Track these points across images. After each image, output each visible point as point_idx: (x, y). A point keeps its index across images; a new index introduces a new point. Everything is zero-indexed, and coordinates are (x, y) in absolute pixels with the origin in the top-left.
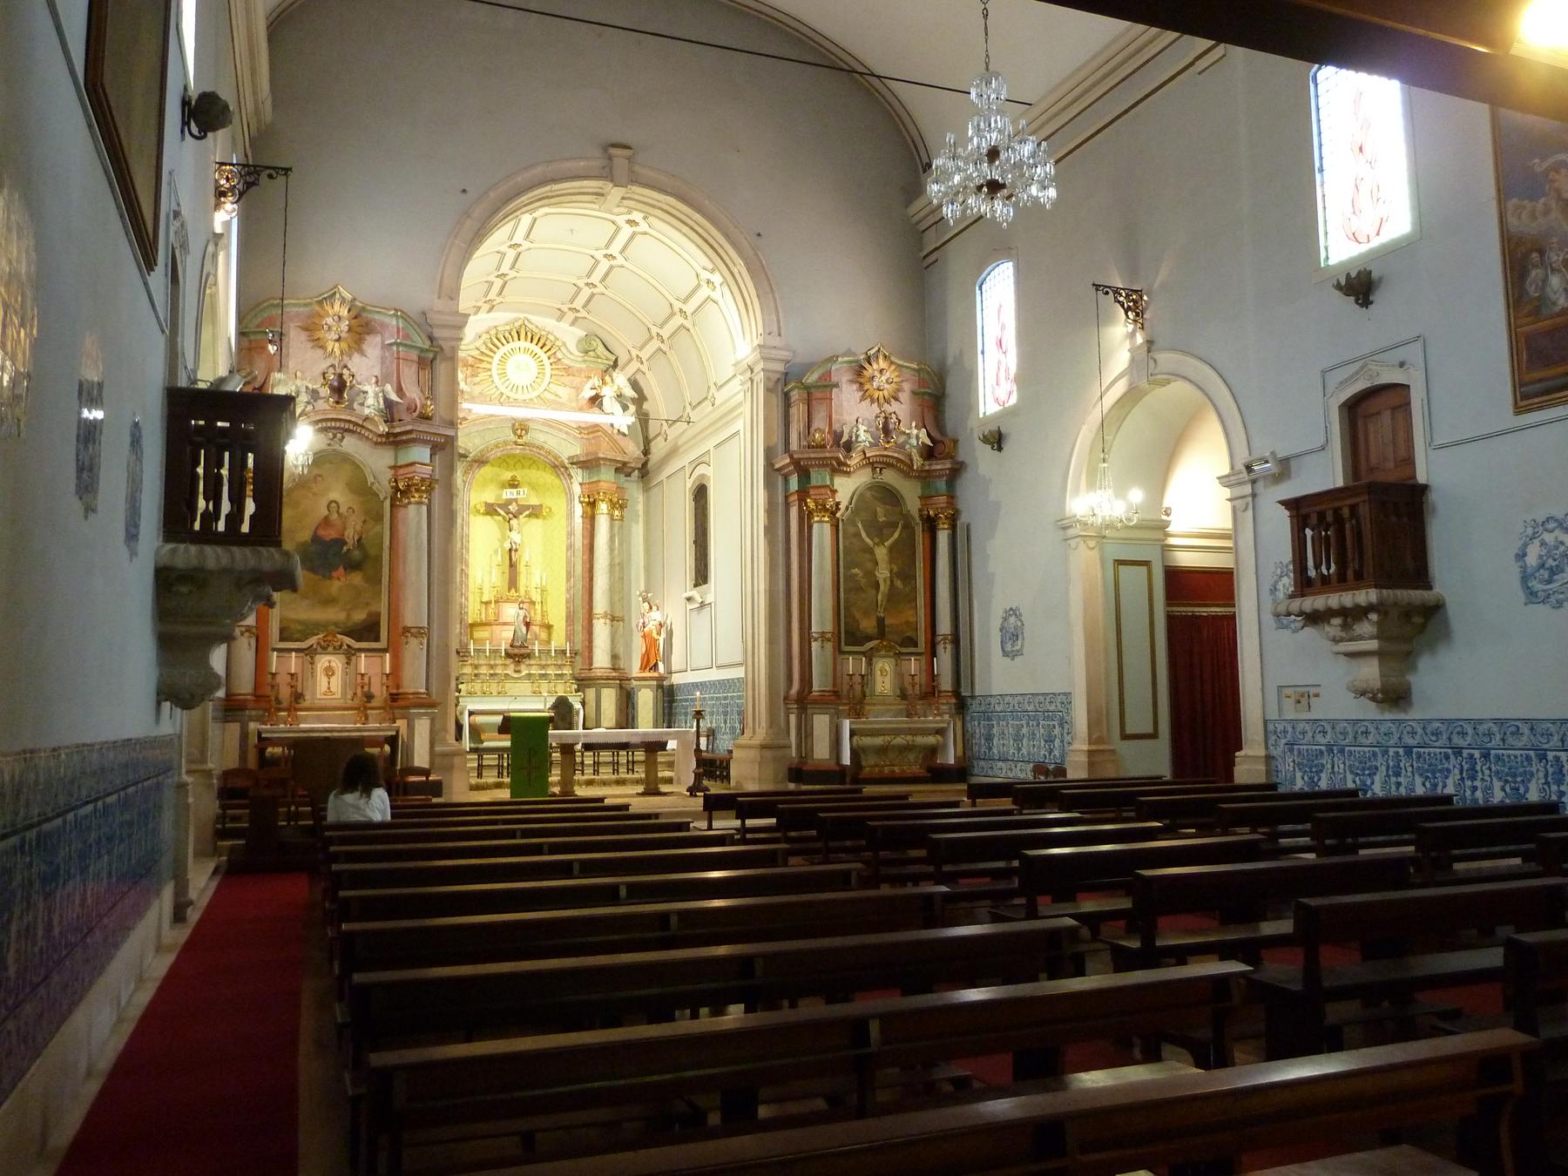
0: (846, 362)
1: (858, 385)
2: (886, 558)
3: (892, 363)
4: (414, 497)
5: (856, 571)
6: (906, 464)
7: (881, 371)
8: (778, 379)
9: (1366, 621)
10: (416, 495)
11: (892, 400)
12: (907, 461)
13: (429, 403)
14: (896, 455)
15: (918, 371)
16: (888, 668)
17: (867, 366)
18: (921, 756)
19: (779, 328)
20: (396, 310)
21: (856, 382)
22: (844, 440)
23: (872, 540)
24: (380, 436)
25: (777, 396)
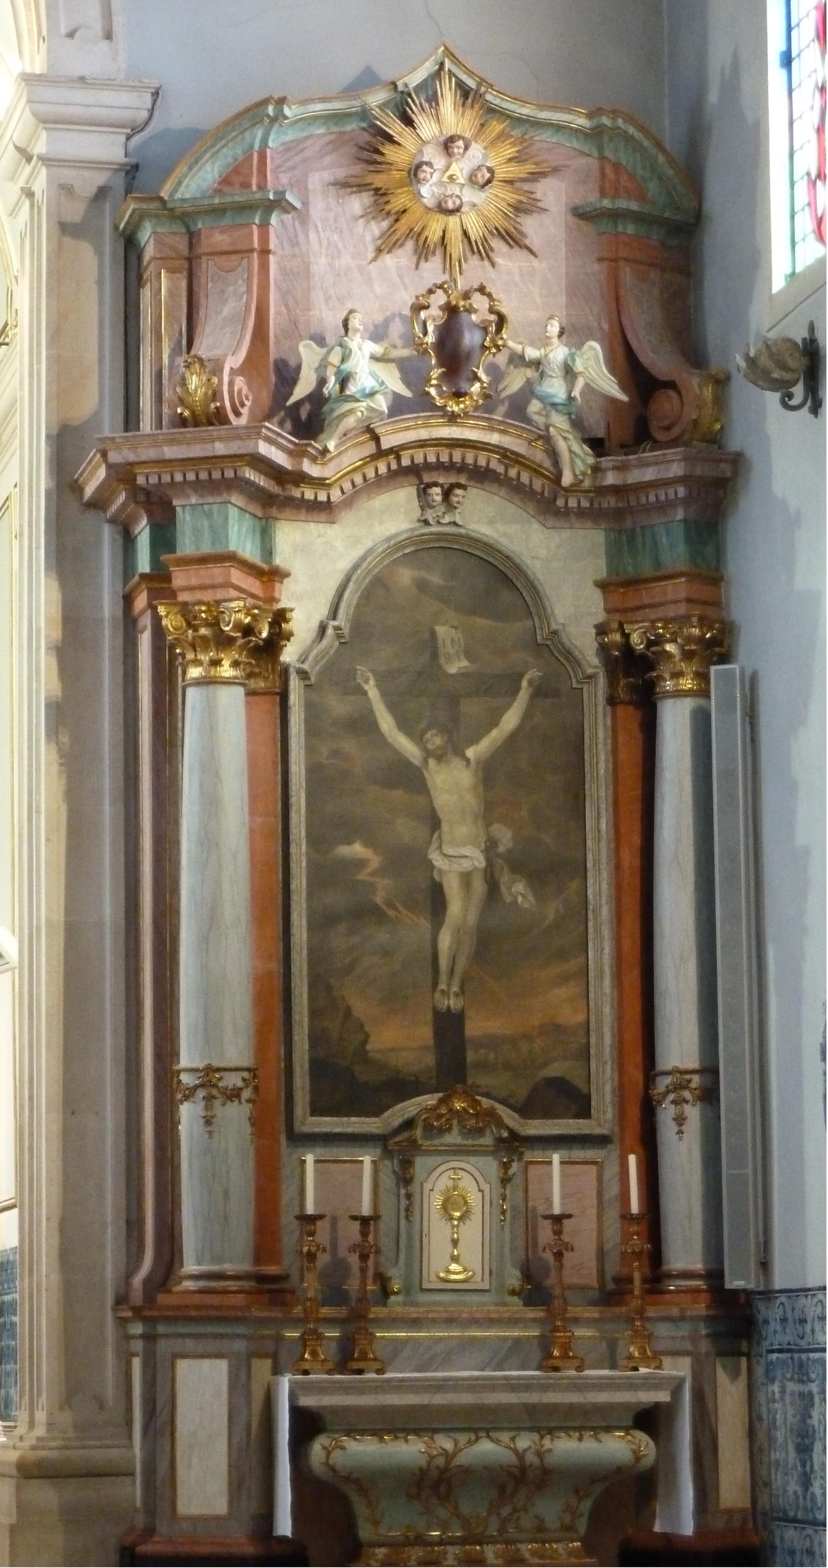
0: (314, 119)
2: (471, 801)
3: (492, 111)
5: (357, 849)
6: (536, 470)
7: (447, 145)
11: (497, 244)
12: (547, 463)
14: (494, 438)
15: (595, 135)
16: (474, 1199)
17: (395, 128)
18: (586, 1506)
21: (362, 187)
22: (301, 391)
23: (418, 738)
25: (99, 253)
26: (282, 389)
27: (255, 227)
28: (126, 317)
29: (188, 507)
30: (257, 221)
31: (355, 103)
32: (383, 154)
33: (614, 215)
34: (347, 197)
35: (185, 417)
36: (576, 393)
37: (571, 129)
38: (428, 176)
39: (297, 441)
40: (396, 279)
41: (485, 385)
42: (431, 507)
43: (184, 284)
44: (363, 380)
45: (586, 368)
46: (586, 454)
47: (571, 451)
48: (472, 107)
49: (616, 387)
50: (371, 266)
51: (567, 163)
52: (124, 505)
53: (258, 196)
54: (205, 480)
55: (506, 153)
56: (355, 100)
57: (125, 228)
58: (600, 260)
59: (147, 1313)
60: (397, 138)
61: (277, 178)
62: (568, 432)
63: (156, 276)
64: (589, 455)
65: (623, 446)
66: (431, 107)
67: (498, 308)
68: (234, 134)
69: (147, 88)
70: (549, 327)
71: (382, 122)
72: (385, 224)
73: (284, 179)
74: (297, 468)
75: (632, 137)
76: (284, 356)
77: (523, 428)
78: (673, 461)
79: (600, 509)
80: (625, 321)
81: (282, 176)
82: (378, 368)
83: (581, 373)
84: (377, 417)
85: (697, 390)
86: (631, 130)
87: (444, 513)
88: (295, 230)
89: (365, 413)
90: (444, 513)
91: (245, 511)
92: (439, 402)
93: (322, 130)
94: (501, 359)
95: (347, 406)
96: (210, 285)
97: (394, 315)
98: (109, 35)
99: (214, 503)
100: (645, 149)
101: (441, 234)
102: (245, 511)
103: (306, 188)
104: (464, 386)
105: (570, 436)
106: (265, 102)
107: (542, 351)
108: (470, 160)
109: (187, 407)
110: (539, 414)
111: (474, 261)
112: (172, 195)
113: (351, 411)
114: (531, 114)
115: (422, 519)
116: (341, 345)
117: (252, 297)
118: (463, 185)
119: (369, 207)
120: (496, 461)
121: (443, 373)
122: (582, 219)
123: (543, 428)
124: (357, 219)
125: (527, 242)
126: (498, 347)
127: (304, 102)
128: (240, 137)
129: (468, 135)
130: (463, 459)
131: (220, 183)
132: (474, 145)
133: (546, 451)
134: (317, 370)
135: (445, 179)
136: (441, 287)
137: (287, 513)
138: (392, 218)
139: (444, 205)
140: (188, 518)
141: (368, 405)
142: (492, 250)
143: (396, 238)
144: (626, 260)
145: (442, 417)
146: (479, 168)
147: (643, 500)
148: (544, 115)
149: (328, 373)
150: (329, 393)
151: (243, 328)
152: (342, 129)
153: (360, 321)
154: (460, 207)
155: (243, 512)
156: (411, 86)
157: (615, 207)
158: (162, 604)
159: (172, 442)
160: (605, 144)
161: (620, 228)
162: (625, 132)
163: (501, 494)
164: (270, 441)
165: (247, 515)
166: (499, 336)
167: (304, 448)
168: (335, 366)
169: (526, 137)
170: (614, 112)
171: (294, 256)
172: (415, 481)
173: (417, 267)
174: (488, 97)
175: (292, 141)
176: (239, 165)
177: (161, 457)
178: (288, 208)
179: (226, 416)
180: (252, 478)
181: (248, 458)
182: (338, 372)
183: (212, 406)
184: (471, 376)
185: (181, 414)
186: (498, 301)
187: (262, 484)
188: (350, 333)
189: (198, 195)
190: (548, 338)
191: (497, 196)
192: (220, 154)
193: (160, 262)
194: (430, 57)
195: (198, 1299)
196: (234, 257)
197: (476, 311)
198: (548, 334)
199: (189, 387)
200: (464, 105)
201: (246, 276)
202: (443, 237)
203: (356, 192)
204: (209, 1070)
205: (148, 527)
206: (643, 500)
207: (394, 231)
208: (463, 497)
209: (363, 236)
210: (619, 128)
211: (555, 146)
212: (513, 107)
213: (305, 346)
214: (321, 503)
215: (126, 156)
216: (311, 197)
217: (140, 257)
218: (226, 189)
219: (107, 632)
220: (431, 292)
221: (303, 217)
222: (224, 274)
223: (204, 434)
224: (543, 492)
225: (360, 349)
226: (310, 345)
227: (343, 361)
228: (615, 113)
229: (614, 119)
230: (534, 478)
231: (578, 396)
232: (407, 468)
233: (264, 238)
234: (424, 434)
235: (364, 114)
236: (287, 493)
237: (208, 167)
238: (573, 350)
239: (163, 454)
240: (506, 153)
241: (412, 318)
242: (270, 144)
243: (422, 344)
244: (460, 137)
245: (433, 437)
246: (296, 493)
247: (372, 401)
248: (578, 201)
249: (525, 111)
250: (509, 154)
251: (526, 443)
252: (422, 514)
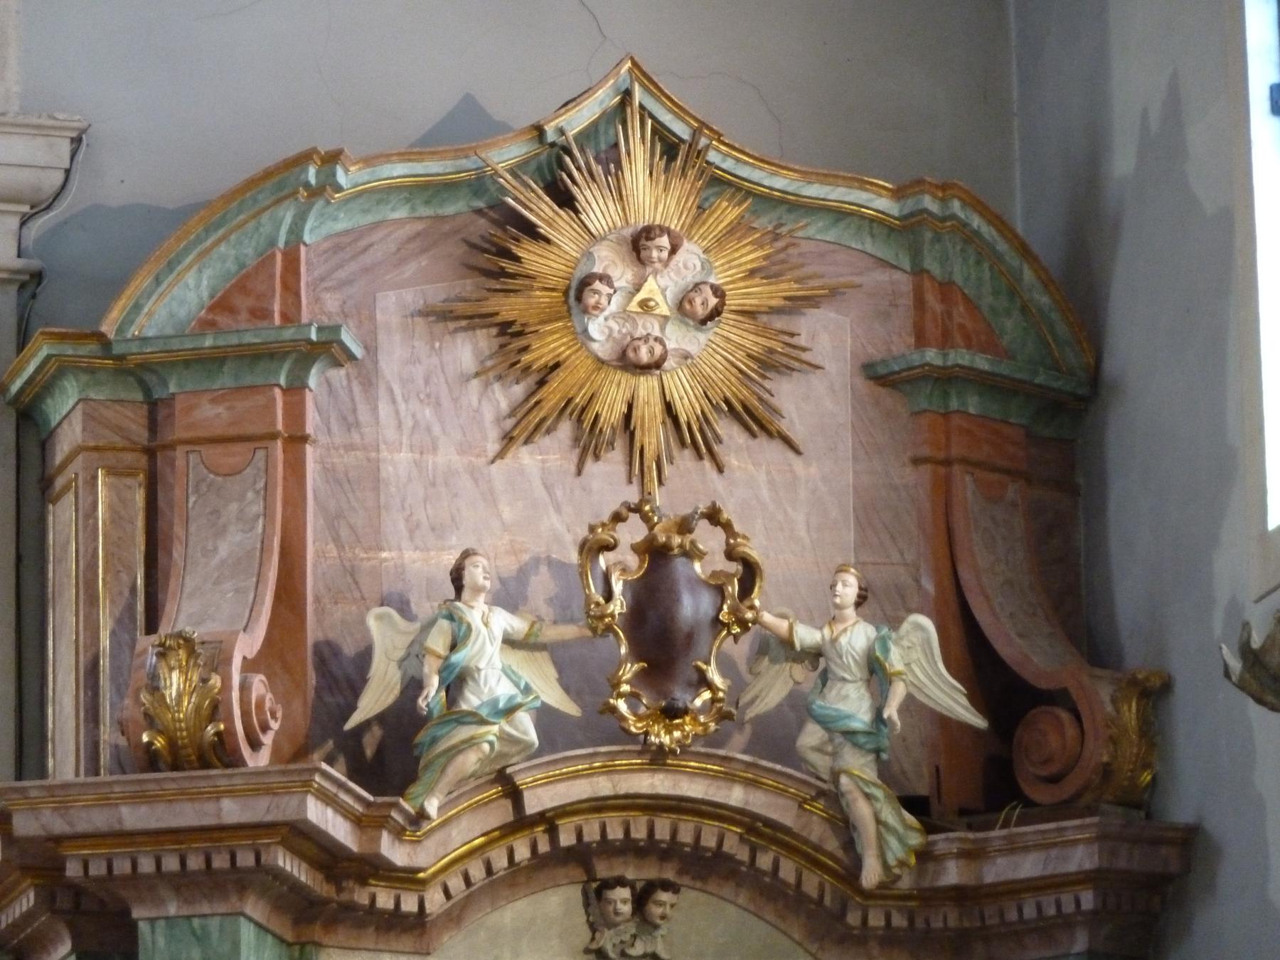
0: (386, 193)
1: (485, 340)
3: (718, 183)
6: (809, 856)
9: (516, 629)
11: (727, 429)
12: (832, 845)
14: (736, 796)
17: (541, 210)
21: (476, 320)
26: (329, 699)
27: (277, 391)
28: (19, 559)
29: (162, 923)
30: (282, 381)
31: (464, 163)
32: (517, 259)
33: (946, 379)
34: (447, 337)
35: (156, 752)
36: (891, 711)
37: (863, 217)
38: (604, 301)
39: (371, 798)
40: (540, 492)
41: (721, 694)
42: (611, 925)
43: (140, 497)
44: (492, 681)
45: (908, 665)
46: (908, 827)
47: (878, 821)
48: (684, 174)
49: (964, 701)
50: (494, 467)
51: (857, 280)
52: (28, 917)
53: (288, 334)
54: (199, 871)
55: (744, 260)
56: (466, 157)
57: (22, 391)
58: (916, 461)
60: (544, 229)
61: (317, 300)
62: (875, 785)
63: (86, 482)
64: (910, 828)
65: (963, 812)
66: (607, 172)
67: (747, 550)
68: (242, 217)
69: (61, 128)
70: (839, 587)
71: (515, 199)
72: (519, 390)
73: (332, 302)
74: (368, 849)
75: (977, 233)
76: (331, 636)
77: (790, 777)
78: (1075, 843)
79: (928, 930)
80: (966, 575)
81: (327, 296)
82: (517, 659)
83: (899, 674)
84: (519, 753)
85: (1109, 708)
86: (976, 222)
87: (634, 937)
88: (353, 400)
89: (497, 746)
90: (634, 937)
91: (267, 930)
92: (635, 727)
93: (402, 213)
94: (740, 650)
95: (464, 733)
96: (192, 499)
97: (537, 561)
99: (213, 915)
100: (999, 257)
101: (625, 409)
102: (267, 930)
103: (372, 318)
104: (681, 696)
105: (879, 793)
106: (302, 159)
107: (826, 631)
108: (678, 272)
109: (160, 732)
110: (819, 749)
111: (685, 459)
112: (120, 330)
113: (471, 743)
114: (790, 189)
115: (594, 946)
116: (451, 617)
117: (273, 523)
118: (666, 318)
119: (491, 357)
120: (737, 838)
121: (643, 670)
122: (883, 385)
123: (826, 777)
124: (468, 380)
125: (784, 426)
126: (744, 624)
127: (369, 161)
128: (252, 224)
129: (674, 225)
130: (674, 833)
131: (211, 309)
132: (686, 245)
133: (830, 821)
134: (401, 662)
135: (634, 307)
136: (637, 509)
137: (341, 935)
138: (532, 380)
139: (631, 354)
140: (161, 942)
141: (501, 730)
142: (719, 440)
143: (542, 414)
144: (964, 461)
145: (640, 754)
146: (696, 287)
147: (1012, 916)
148: (814, 191)
149: (426, 669)
150: (428, 706)
152: (440, 212)
153: (485, 570)
154: (663, 358)
155: (262, 933)
156: (571, 133)
157: (949, 363)
159: (139, 798)
160: (926, 247)
161: (954, 404)
162: (965, 225)
163: (741, 901)
164: (328, 799)
165: (270, 938)
166: (747, 603)
167: (384, 812)
168: (439, 657)
169: (784, 230)
170: (944, 187)
171: (350, 447)
172: (579, 874)
173: (579, 472)
174: (712, 156)
175: (347, 232)
176: (247, 276)
177: (117, 827)
178: (341, 357)
179: (236, 751)
180: (288, 868)
181: (284, 830)
182: (445, 670)
183: (210, 730)
184: (695, 677)
185: (150, 744)
186: (745, 537)
187: (303, 879)
188: (466, 594)
189: (169, 331)
190: (839, 607)
191: (728, 340)
192: (214, 255)
193: (95, 455)
194: (605, 78)
196: (238, 448)
197: (701, 555)
198: (838, 600)
199: (167, 693)
200: (667, 169)
201: (261, 484)
202: (628, 417)
203: (465, 329)
206: (1012, 916)
207: (537, 403)
208: (672, 906)
209: (477, 411)
210: (953, 217)
211: (832, 247)
212: (756, 175)
213: (380, 618)
214: (407, 915)
215: (19, 256)
216: (382, 337)
217: (45, 444)
218: (223, 320)
220: (617, 518)
221: (368, 378)
222: (220, 479)
223: (203, 783)
224: (822, 896)
225: (486, 624)
226: (390, 616)
227: (453, 647)
228: (945, 190)
229: (944, 201)
230: (805, 873)
231: (895, 717)
232: (569, 849)
233: (296, 414)
234: (603, 786)
235: (480, 183)
236: (344, 897)
237: (190, 278)
238: (885, 631)
239: (120, 821)
240: (744, 260)
241: (582, 566)
242: (307, 238)
243: (602, 617)
244: (664, 230)
245: (622, 792)
246: (361, 897)
247: (510, 723)
248: (875, 353)
249: (780, 182)
250: (752, 261)
251: (793, 806)
252: (593, 939)
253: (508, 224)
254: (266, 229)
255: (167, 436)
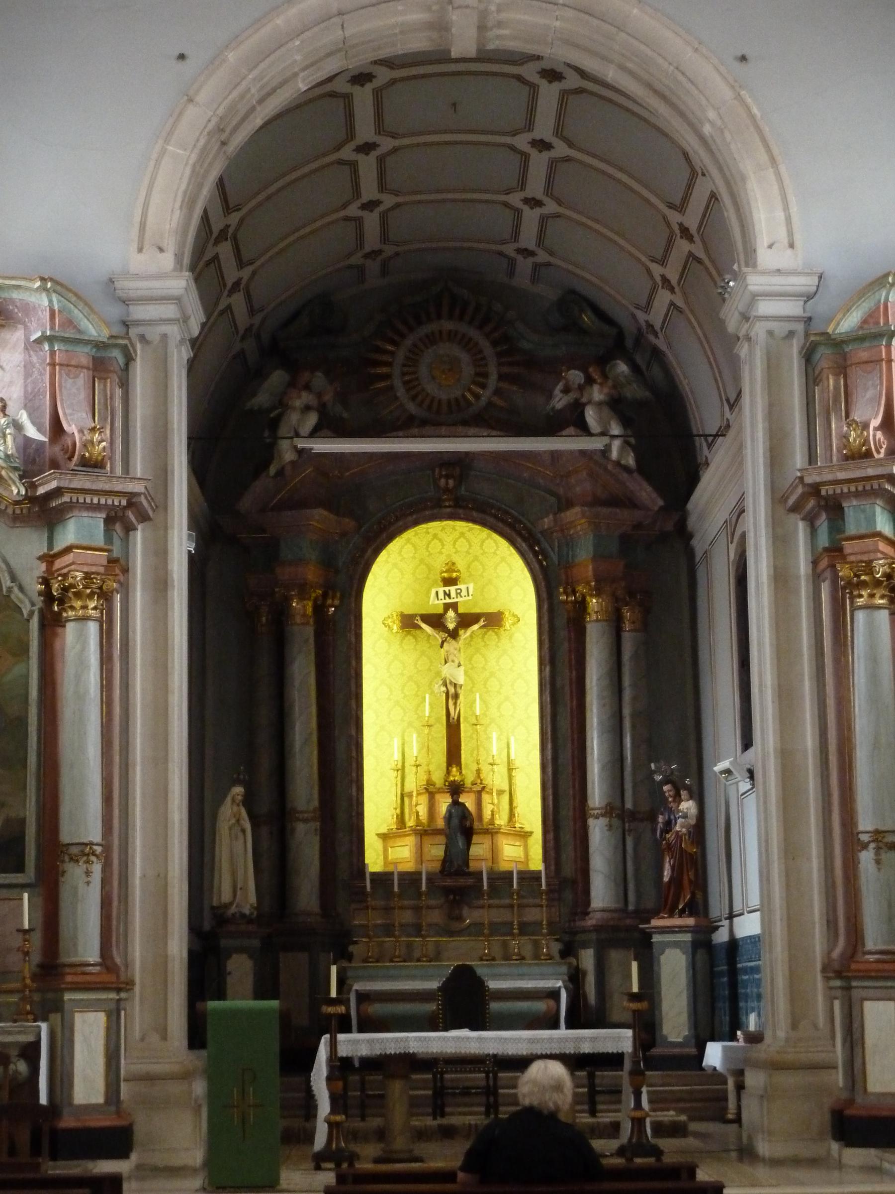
4: (72, 608)
8: (791, 334)
10: (78, 604)
13: (96, 437)
19: (790, 233)
20: (43, 279)
24: (17, 503)
30: (884, 343)
53: (885, 328)
59: (845, 974)
98: (792, 246)
140: (851, 513)
151: (879, 404)
158: (839, 563)
159: (841, 469)
183: (864, 448)
195: (874, 966)
196: (871, 364)
204: (877, 832)
205: (826, 521)
218: (866, 326)
219: (803, 583)
233: (889, 352)
237: (854, 314)
253: (392, 892)
254: (877, 297)
255: (849, 363)
